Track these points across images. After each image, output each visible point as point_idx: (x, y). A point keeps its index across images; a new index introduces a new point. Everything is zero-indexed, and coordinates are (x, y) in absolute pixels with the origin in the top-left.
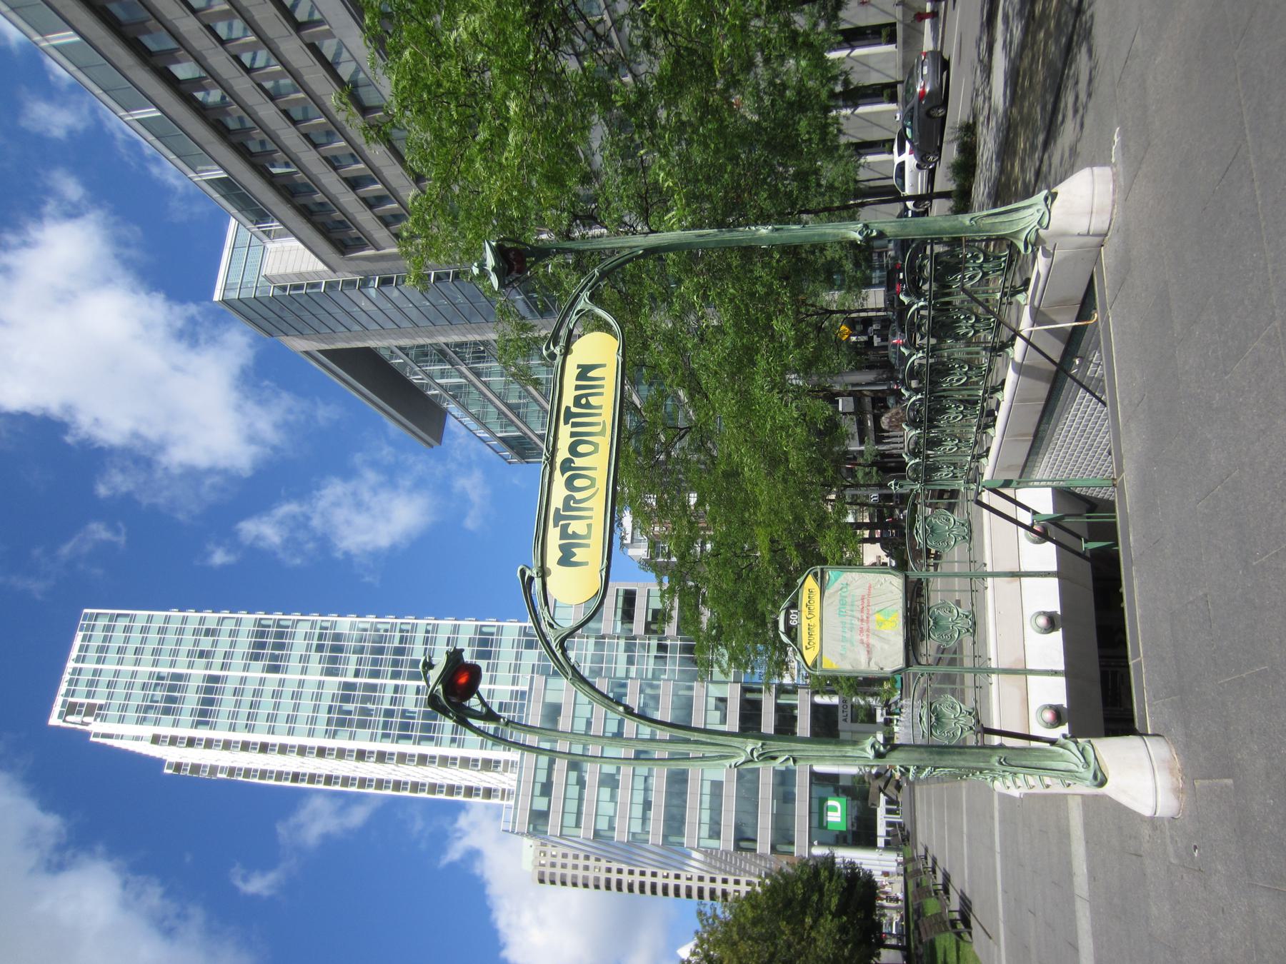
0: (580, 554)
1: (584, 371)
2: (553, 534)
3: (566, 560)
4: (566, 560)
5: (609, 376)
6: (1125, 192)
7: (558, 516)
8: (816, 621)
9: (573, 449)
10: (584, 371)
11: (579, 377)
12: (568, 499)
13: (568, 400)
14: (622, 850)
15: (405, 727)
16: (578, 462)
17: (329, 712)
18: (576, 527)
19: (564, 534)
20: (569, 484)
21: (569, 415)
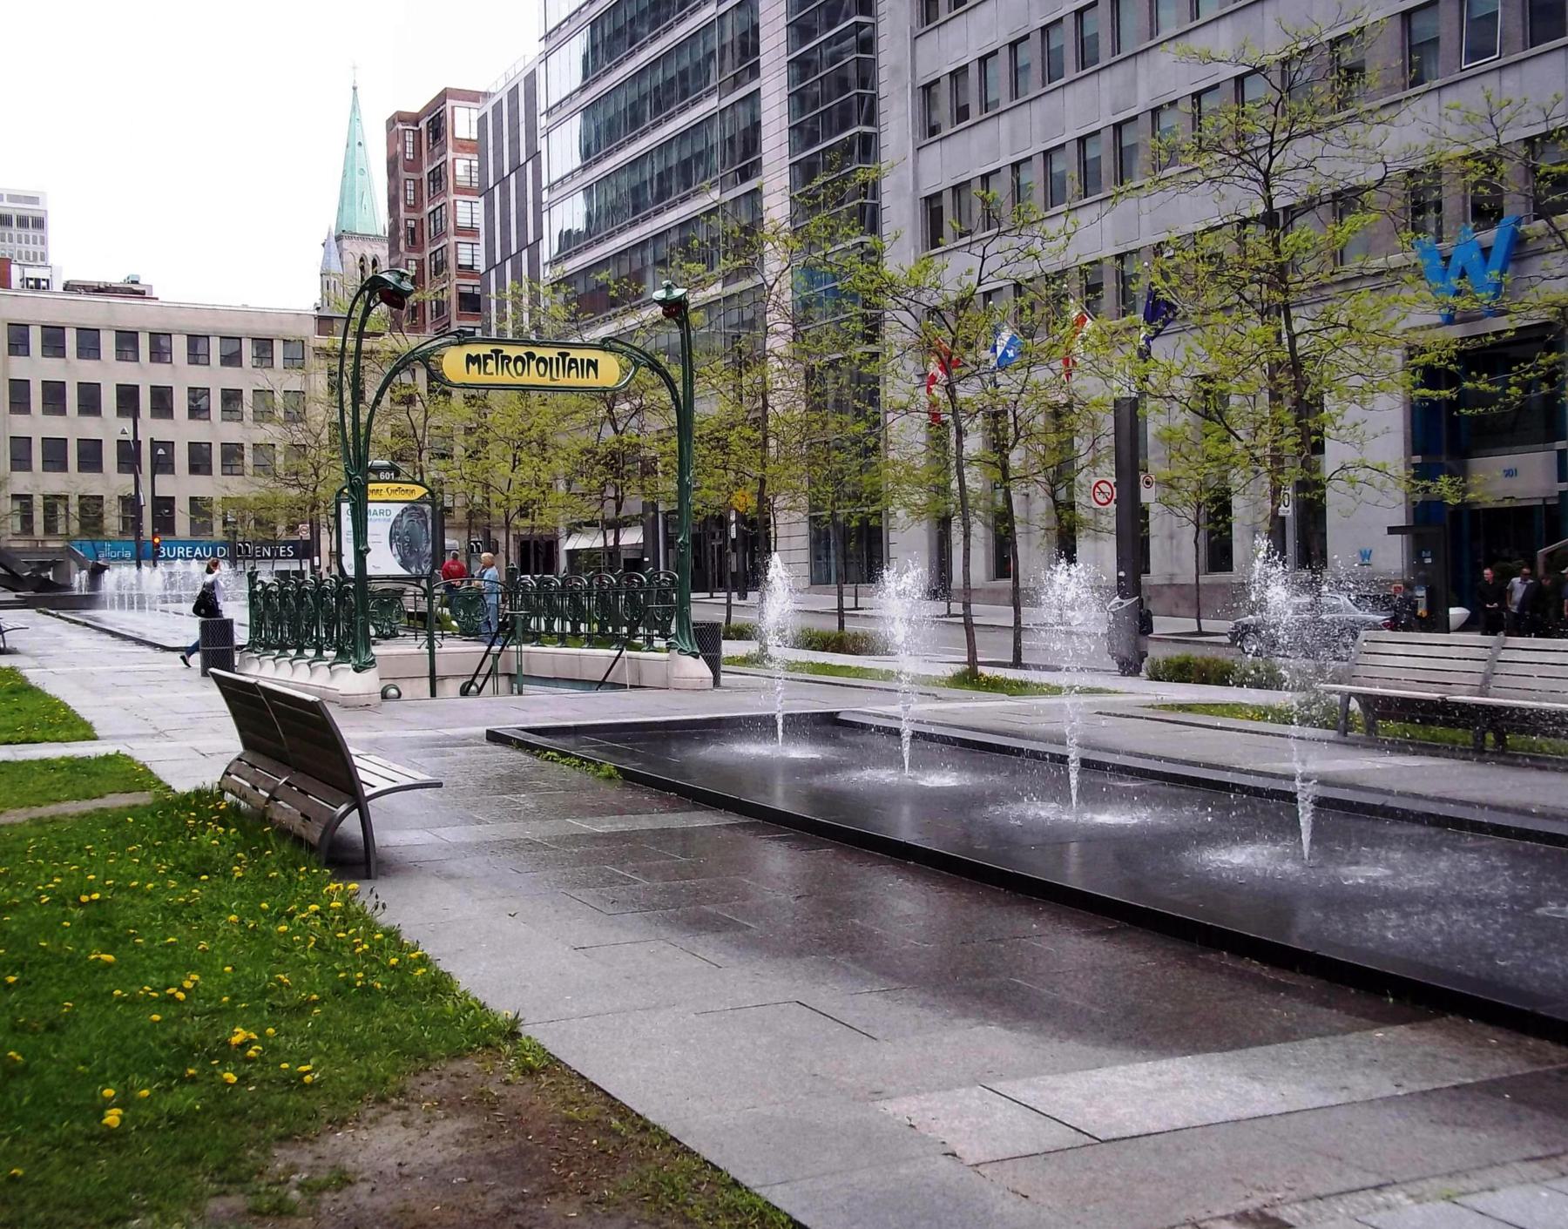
0: (474, 368)
1: (593, 364)
2: (486, 350)
3: (471, 359)
4: (471, 359)
5: (590, 380)
7: (497, 352)
9: (542, 359)
10: (593, 364)
12: (509, 358)
16: (533, 364)
19: (486, 357)
20: (519, 358)
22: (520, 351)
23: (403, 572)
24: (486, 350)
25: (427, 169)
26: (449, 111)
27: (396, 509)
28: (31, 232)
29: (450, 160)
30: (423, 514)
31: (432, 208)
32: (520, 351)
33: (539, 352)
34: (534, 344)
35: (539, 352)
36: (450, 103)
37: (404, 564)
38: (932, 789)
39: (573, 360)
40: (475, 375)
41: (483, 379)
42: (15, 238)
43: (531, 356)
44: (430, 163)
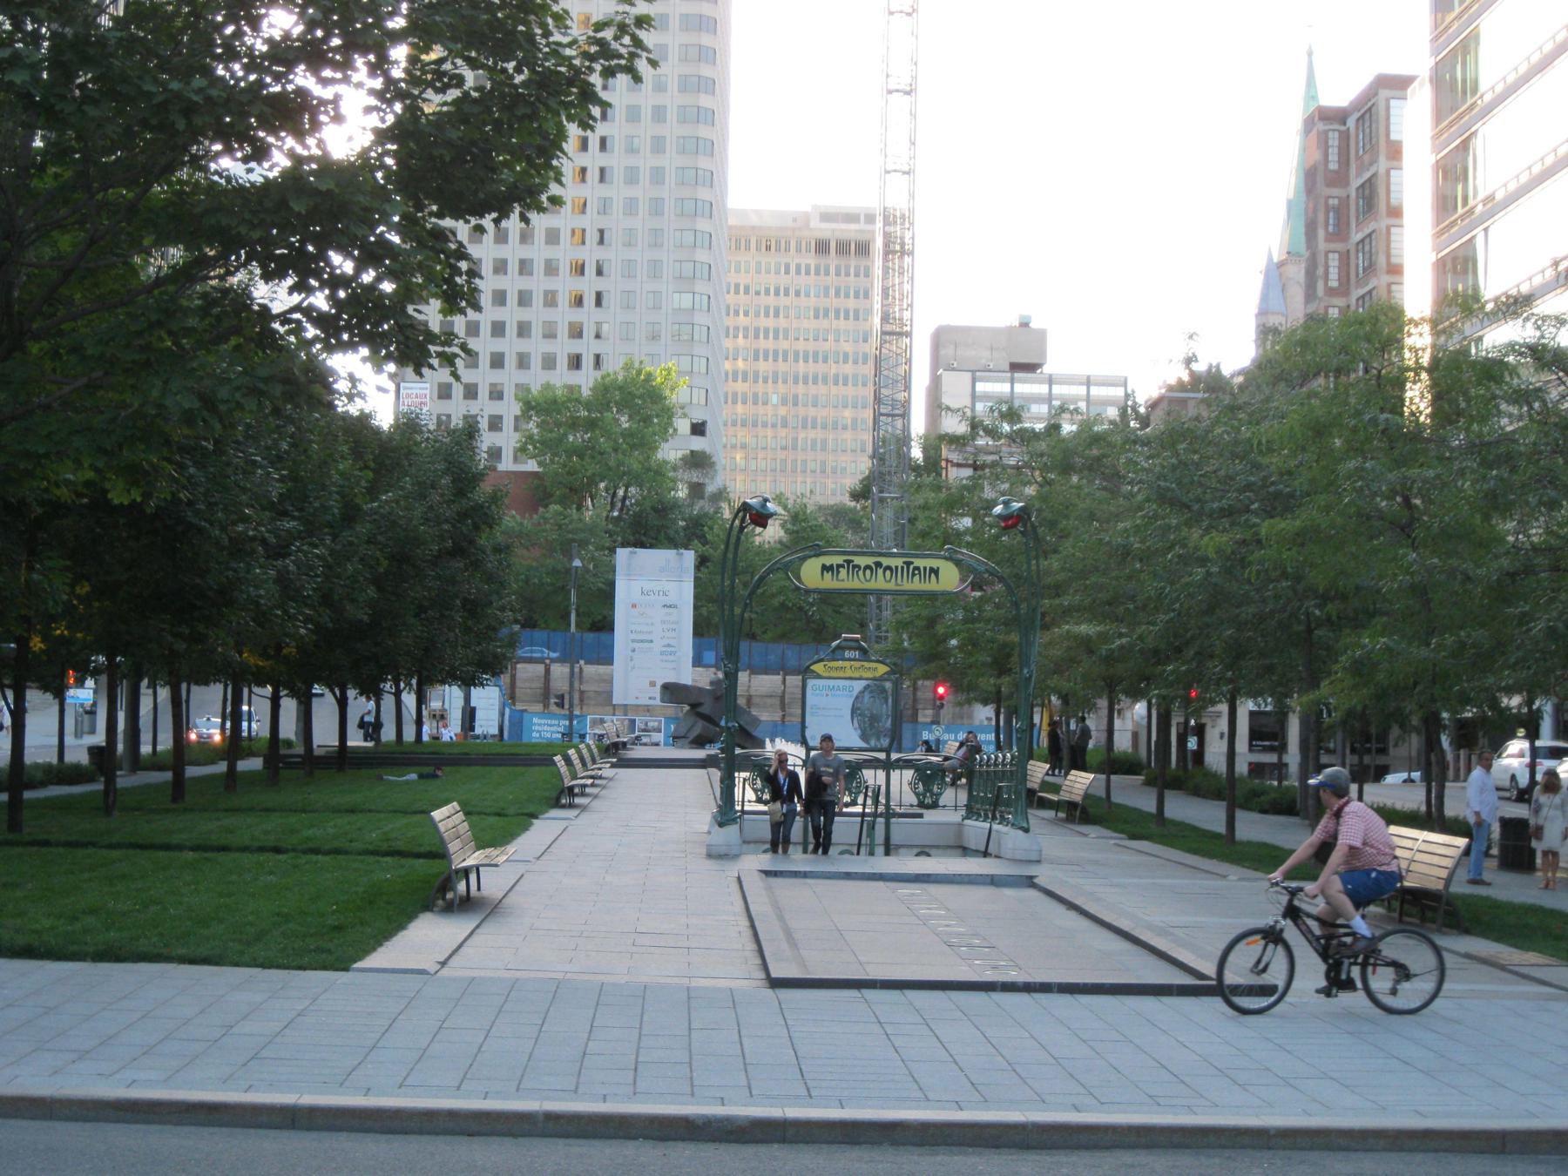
0: (828, 576)
1: (935, 571)
2: (839, 560)
3: (825, 568)
4: (825, 568)
5: (932, 585)
6: (395, 291)
7: (848, 562)
8: (849, 673)
9: (889, 568)
10: (935, 571)
11: (932, 570)
12: (859, 567)
13: (918, 562)
14: (1464, 81)
15: (605, 51)
16: (880, 571)
17: (656, 232)
18: (843, 572)
19: (839, 566)
20: (867, 567)
21: (908, 564)
22: (870, 561)
23: (864, 745)
24: (839, 560)
25: (1356, 183)
26: (1382, 105)
27: (859, 686)
28: (853, 262)
29: (1382, 170)
30: (884, 691)
31: (1359, 236)
32: (870, 561)
33: (885, 561)
34: (881, 555)
35: (885, 561)
36: (1383, 93)
37: (864, 737)
38: (1528, 949)
39: (917, 568)
40: (828, 582)
41: (835, 585)
42: (832, 270)
43: (878, 564)
44: (1358, 175)
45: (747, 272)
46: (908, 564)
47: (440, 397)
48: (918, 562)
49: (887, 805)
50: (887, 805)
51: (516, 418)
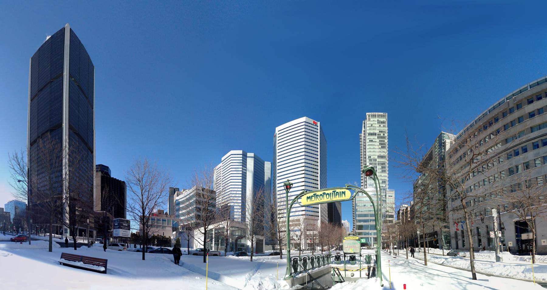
0: (309, 200)
1: (344, 193)
2: (312, 194)
3: (308, 198)
4: (308, 198)
7: (315, 194)
9: (328, 194)
10: (344, 193)
16: (325, 196)
20: (321, 195)
24: (312, 194)
39: (338, 193)
40: (309, 202)
45: (426, 242)
46: (334, 192)
47: (538, 147)
48: (338, 191)
49: (371, 215)
50: (371, 215)
51: (368, 249)
